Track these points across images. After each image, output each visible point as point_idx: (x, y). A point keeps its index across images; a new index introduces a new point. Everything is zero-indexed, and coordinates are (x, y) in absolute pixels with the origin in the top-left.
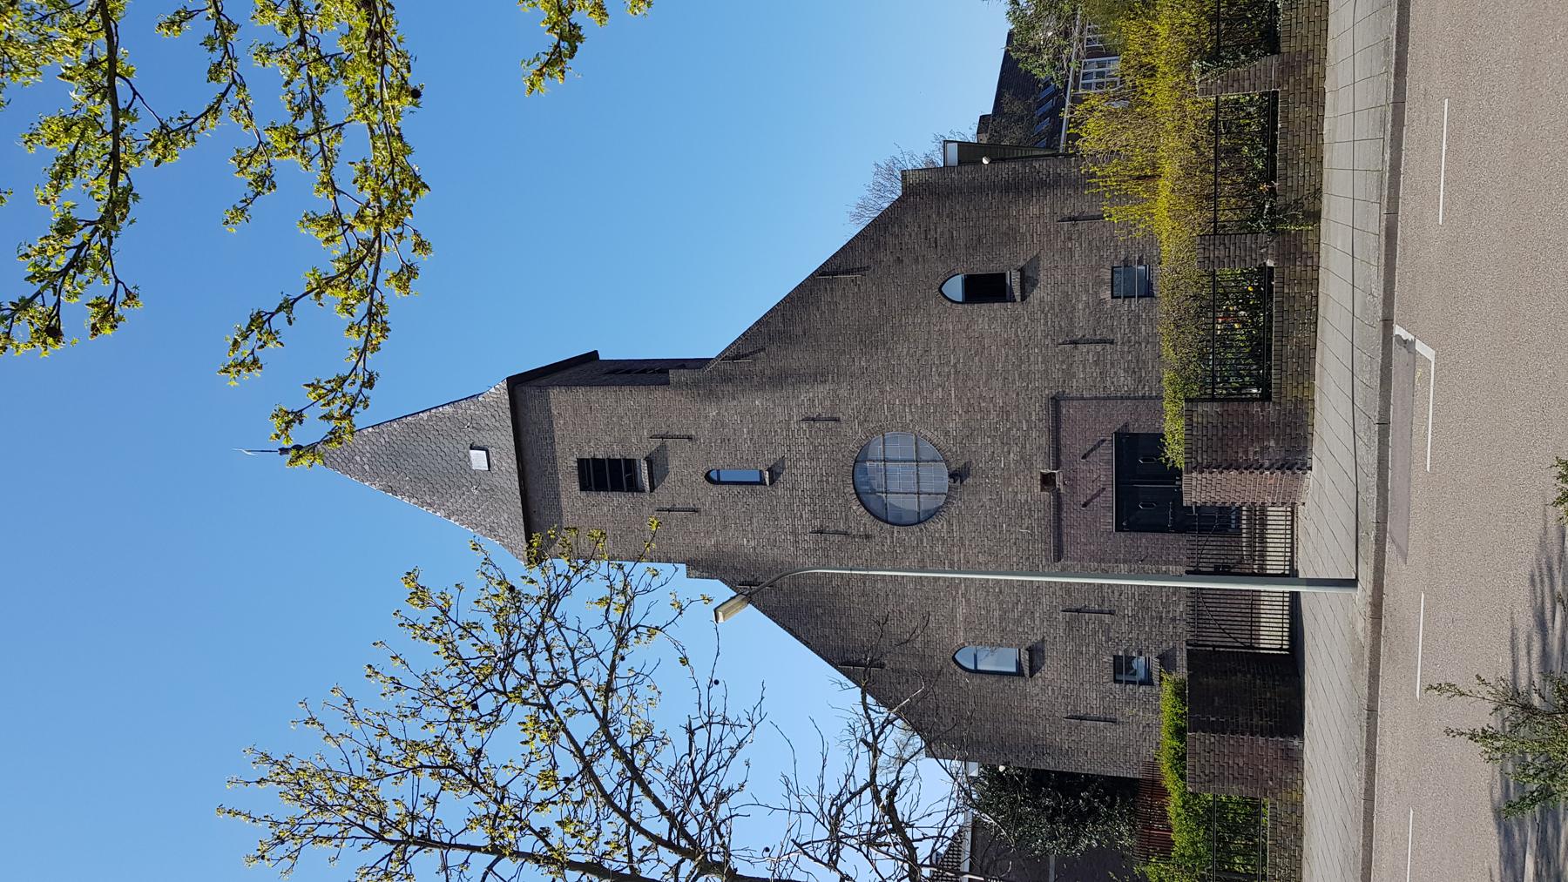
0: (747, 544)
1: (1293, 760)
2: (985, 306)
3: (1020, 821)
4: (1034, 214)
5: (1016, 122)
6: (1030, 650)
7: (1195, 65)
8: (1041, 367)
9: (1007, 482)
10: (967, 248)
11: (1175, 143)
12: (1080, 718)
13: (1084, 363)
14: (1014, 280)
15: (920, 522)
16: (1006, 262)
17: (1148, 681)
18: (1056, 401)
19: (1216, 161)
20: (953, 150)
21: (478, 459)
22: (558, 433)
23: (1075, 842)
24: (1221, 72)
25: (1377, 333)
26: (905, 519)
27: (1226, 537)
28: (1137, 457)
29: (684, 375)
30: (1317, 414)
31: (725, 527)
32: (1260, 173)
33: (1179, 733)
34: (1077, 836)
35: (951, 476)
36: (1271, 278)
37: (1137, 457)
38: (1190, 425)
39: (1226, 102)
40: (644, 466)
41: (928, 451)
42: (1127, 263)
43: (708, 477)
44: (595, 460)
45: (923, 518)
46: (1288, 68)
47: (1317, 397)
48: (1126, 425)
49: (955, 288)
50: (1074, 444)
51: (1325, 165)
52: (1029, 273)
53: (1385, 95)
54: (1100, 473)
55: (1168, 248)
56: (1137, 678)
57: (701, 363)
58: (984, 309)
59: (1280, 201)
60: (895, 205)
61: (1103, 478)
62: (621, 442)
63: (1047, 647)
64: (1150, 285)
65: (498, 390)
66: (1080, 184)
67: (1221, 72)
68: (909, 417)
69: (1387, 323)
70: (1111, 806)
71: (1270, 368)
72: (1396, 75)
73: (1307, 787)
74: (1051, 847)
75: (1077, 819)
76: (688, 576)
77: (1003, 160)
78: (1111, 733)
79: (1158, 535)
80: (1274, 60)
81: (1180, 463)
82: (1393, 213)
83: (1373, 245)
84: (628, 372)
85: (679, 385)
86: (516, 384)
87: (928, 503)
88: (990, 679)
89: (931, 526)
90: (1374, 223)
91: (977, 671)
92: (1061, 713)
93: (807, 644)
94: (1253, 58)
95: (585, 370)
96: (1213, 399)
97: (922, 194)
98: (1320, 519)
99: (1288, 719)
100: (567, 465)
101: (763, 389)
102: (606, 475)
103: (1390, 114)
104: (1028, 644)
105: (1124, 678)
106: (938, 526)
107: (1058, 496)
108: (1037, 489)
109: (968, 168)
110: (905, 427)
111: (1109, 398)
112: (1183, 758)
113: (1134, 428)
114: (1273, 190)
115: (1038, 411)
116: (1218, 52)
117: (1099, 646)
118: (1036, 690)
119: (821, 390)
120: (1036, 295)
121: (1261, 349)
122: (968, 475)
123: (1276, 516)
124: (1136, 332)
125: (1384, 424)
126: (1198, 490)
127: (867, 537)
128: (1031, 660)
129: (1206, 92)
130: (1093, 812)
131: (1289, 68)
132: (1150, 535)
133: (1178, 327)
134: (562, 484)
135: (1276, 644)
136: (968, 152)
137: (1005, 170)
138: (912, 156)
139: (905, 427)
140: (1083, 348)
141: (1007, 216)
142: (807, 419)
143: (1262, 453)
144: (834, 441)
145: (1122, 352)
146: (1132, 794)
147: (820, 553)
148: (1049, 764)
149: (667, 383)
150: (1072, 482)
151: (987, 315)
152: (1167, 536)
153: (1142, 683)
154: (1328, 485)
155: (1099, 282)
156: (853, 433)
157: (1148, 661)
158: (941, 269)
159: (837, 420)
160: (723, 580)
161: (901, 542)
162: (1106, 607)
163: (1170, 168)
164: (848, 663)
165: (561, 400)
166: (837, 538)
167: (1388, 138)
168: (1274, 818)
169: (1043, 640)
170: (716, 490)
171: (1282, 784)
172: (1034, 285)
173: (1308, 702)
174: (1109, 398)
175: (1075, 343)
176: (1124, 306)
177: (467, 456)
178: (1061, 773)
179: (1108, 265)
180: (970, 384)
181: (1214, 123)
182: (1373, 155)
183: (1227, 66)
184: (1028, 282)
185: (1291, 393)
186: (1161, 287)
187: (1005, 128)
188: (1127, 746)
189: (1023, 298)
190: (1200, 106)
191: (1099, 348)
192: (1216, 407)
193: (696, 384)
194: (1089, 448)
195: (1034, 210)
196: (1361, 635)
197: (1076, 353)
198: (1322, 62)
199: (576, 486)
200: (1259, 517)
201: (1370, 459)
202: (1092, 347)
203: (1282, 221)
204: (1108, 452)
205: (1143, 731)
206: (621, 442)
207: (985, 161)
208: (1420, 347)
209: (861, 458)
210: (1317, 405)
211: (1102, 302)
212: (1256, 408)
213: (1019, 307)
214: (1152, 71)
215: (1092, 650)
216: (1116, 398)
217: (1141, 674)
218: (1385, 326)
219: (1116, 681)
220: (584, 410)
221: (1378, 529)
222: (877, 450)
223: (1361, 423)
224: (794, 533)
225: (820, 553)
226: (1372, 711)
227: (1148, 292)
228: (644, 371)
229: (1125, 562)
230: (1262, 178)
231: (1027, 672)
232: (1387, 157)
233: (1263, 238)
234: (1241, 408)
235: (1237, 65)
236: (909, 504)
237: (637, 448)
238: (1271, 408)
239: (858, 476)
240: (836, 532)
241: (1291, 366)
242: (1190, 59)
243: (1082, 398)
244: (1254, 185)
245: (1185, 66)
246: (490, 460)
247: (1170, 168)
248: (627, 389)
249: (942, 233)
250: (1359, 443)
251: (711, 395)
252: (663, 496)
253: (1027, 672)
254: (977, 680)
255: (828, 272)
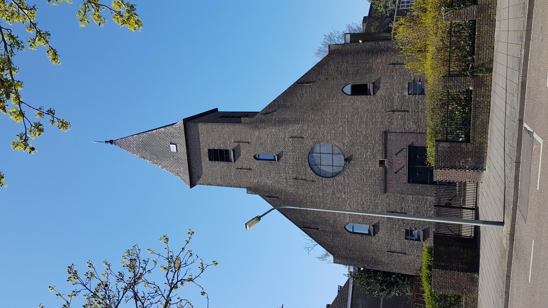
0: (269, 182)
1: (475, 282)
2: (359, 96)
3: (368, 284)
4: (379, 62)
5: (377, 20)
6: (374, 226)
7: (443, 9)
8: (380, 120)
9: (366, 163)
10: (353, 74)
11: (433, 38)
12: (392, 252)
13: (397, 119)
14: (370, 87)
15: (333, 177)
16: (368, 80)
17: (418, 239)
18: (386, 133)
19: (450, 47)
20: (348, 37)
21: (173, 148)
22: (201, 140)
23: (390, 293)
24: (453, 12)
25: (516, 124)
26: (328, 175)
27: (452, 199)
28: (416, 154)
29: (246, 120)
30: (488, 149)
31: (261, 176)
32: (468, 52)
33: (429, 267)
34: (390, 291)
35: (345, 160)
36: (471, 94)
37: (416, 154)
38: (437, 151)
39: (455, 23)
40: (232, 152)
41: (336, 150)
42: (414, 81)
43: (255, 157)
44: (214, 149)
45: (334, 175)
46: (481, 10)
47: (489, 142)
48: (413, 143)
49: (348, 89)
50: (392, 149)
51: (495, 50)
52: (376, 84)
53: (523, 26)
54: (401, 161)
55: (430, 80)
56: (414, 238)
57: (255, 113)
58: (359, 98)
59: (476, 64)
60: (324, 59)
61: (403, 163)
62: (224, 143)
63: (380, 225)
64: (423, 90)
65: (180, 124)
66: (396, 51)
67: (453, 12)
68: (330, 138)
69: (521, 121)
70: (403, 281)
71: (470, 129)
72: (528, 19)
73: (479, 293)
74: (382, 295)
75: (391, 285)
76: (247, 193)
77: (368, 41)
78: (404, 258)
79: (425, 185)
80: (475, 7)
81: (433, 164)
82: (524, 76)
83: (515, 88)
84: (227, 117)
85: (245, 124)
86: (186, 121)
87: (336, 170)
88: (358, 236)
89: (337, 178)
90: (516, 78)
91: (353, 233)
92: (385, 249)
93: (290, 220)
94: (466, 6)
95: (213, 116)
96: (447, 141)
97: (335, 54)
98: (489, 191)
99: (473, 266)
100: (204, 152)
101: (275, 126)
102: (219, 155)
103: (524, 35)
104: (373, 224)
105: (409, 237)
106: (340, 178)
107: (386, 169)
108: (378, 166)
109: (354, 44)
110: (328, 141)
111: (406, 133)
112: (431, 277)
113: (416, 144)
114: (473, 59)
115: (378, 137)
116: (452, 4)
117: (400, 225)
118: (376, 241)
119: (297, 126)
120: (379, 93)
121: (466, 123)
122: (351, 160)
123: (470, 188)
124: (417, 107)
125: (518, 163)
126: (439, 175)
127: (313, 181)
128: (374, 229)
129: (447, 20)
130: (396, 283)
131: (481, 10)
132: (421, 185)
133: (433, 111)
134: (203, 158)
135: (468, 234)
136: (355, 37)
137: (368, 45)
138: (338, 32)
139: (328, 141)
140: (397, 113)
141: (369, 63)
142: (291, 137)
143: (466, 164)
144: (302, 145)
145: (412, 115)
146: (413, 280)
147: (295, 186)
148: (380, 268)
149: (241, 122)
150: (391, 164)
151: (360, 101)
152: (427, 186)
153: (416, 240)
154: (492, 179)
155: (403, 89)
156: (308, 143)
157: (418, 232)
158: (343, 82)
159: (303, 138)
160: (260, 195)
161: (326, 184)
162: (403, 211)
163: (431, 49)
164: (305, 227)
165: (202, 128)
166: (302, 181)
167: (524, 44)
168: (466, 303)
169: (379, 222)
170: (257, 162)
171: (470, 291)
172: (378, 89)
173: (481, 260)
174: (406, 133)
175: (394, 111)
176: (413, 98)
177: (169, 146)
178: (385, 272)
179: (407, 82)
180: (353, 126)
181: (450, 32)
182: (517, 51)
183: (456, 9)
184: (376, 88)
185: (478, 140)
186: (428, 89)
187: (372, 22)
188: (409, 263)
189: (374, 94)
190: (444, 24)
191: (403, 113)
192: (448, 144)
193: (251, 123)
194: (398, 151)
195: (379, 60)
196: (505, 246)
197: (394, 115)
198: (495, 8)
199: (207, 159)
200: (463, 185)
201: (511, 176)
202: (400, 113)
203: (476, 72)
204: (406, 153)
205: (418, 258)
206: (224, 143)
207: (360, 41)
208: (535, 135)
209: (311, 152)
210: (489, 145)
211: (404, 96)
212: (464, 145)
213: (372, 97)
214: (425, 10)
215: (397, 227)
216: (409, 133)
217: (416, 237)
218: (520, 122)
219: (406, 239)
220: (211, 131)
221: (514, 203)
222: (317, 149)
223: (508, 160)
224: (286, 179)
225: (295, 186)
226: (508, 277)
227: (422, 92)
228: (233, 117)
229: (411, 194)
230: (469, 56)
231: (372, 234)
232: (523, 53)
233: (469, 78)
234: (458, 145)
235: (460, 9)
236: (329, 170)
237: (230, 146)
238: (469, 145)
239: (310, 158)
240: (302, 179)
241: (479, 129)
242: (441, 6)
243: (396, 132)
244: (466, 57)
245: (438, 9)
246: (177, 148)
247: (431, 49)
248: (226, 124)
249: (343, 69)
250: (506, 168)
251: (256, 127)
252: (238, 164)
253: (372, 234)
254: (353, 236)
255: (300, 83)
